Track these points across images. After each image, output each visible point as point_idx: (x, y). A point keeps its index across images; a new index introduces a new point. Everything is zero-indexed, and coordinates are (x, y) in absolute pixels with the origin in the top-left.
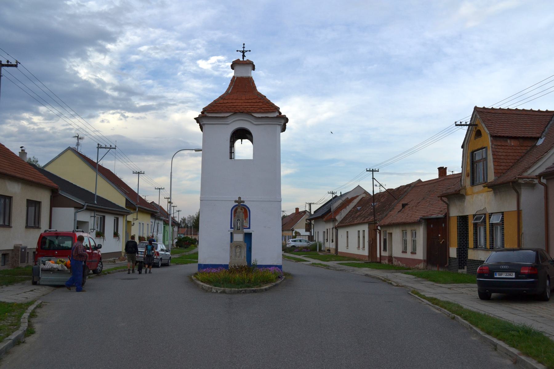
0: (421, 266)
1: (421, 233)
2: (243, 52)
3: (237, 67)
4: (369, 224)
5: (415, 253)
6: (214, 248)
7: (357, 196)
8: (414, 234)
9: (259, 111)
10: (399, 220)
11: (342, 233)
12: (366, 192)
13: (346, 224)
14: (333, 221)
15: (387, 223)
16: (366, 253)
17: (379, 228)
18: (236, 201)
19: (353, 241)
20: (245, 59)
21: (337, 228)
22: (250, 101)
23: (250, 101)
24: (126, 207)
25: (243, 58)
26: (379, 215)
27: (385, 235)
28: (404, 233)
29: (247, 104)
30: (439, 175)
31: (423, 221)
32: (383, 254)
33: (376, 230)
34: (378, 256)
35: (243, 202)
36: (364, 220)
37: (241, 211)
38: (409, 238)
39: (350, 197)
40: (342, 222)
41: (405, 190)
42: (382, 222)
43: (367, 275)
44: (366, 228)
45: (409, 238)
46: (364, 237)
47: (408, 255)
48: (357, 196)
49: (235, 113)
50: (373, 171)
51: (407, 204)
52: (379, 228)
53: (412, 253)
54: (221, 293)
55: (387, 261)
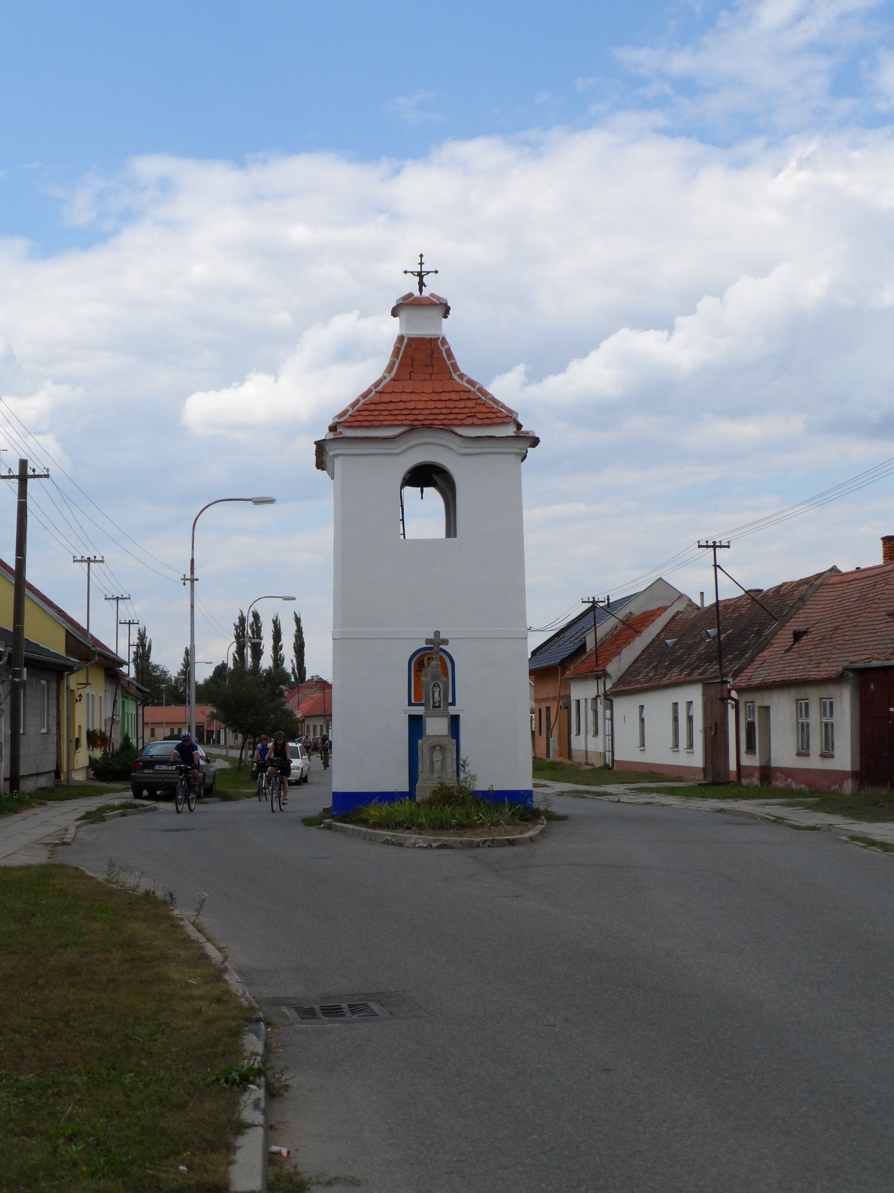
0: (848, 786)
1: (845, 703)
2: (420, 275)
3: (403, 313)
4: (706, 685)
5: (832, 757)
6: (367, 752)
7: (664, 609)
8: (828, 708)
9: (469, 421)
10: (789, 674)
11: (626, 708)
12: (691, 604)
13: (632, 684)
14: (598, 678)
15: (756, 681)
16: (697, 760)
17: (734, 694)
18: (428, 641)
19: (658, 728)
20: (426, 292)
21: (609, 698)
22: (445, 396)
23: (445, 396)
24: (68, 651)
25: (421, 290)
26: (731, 662)
27: (750, 712)
28: (803, 709)
29: (439, 405)
30: (885, 555)
31: (851, 675)
32: (746, 761)
33: (724, 700)
34: (733, 766)
35: (445, 642)
36: (690, 674)
37: (430, 667)
38: (814, 719)
39: (636, 609)
40: (624, 679)
41: (797, 594)
42: (742, 681)
43: (722, 811)
44: (695, 695)
45: (814, 719)
46: (690, 719)
47: (814, 762)
48: (664, 609)
49: (413, 429)
50: (714, 546)
51: (804, 633)
52: (734, 694)
53: (823, 756)
54: (439, 847)
55: (756, 781)
